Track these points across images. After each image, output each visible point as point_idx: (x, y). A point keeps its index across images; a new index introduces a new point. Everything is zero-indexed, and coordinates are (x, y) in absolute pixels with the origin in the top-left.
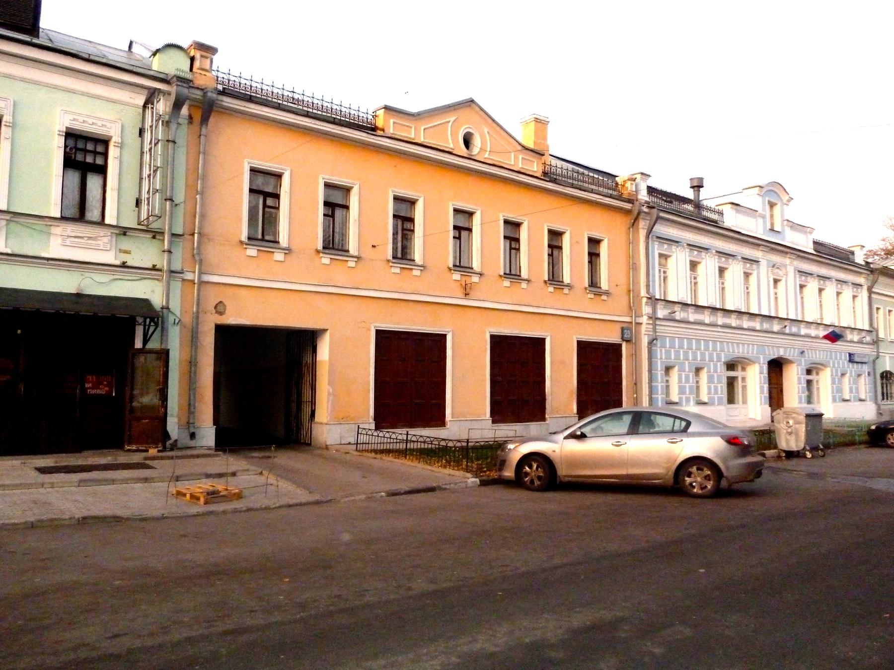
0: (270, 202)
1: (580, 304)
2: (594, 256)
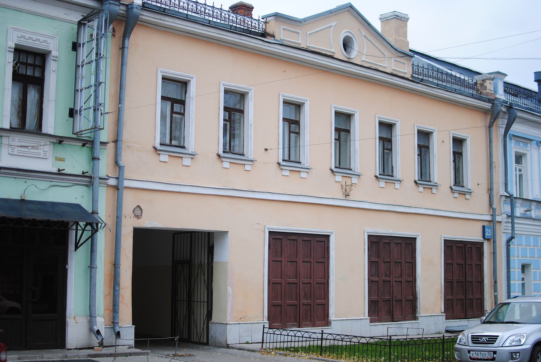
1: (443, 200)
2: (458, 155)
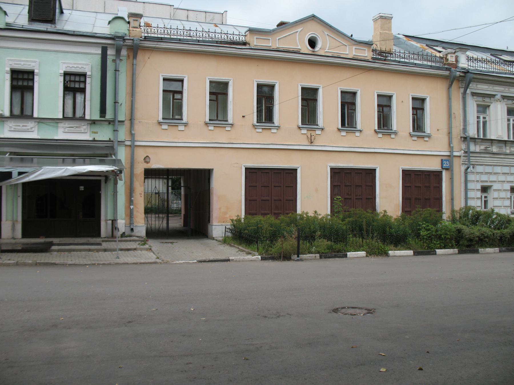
0: (177, 96)
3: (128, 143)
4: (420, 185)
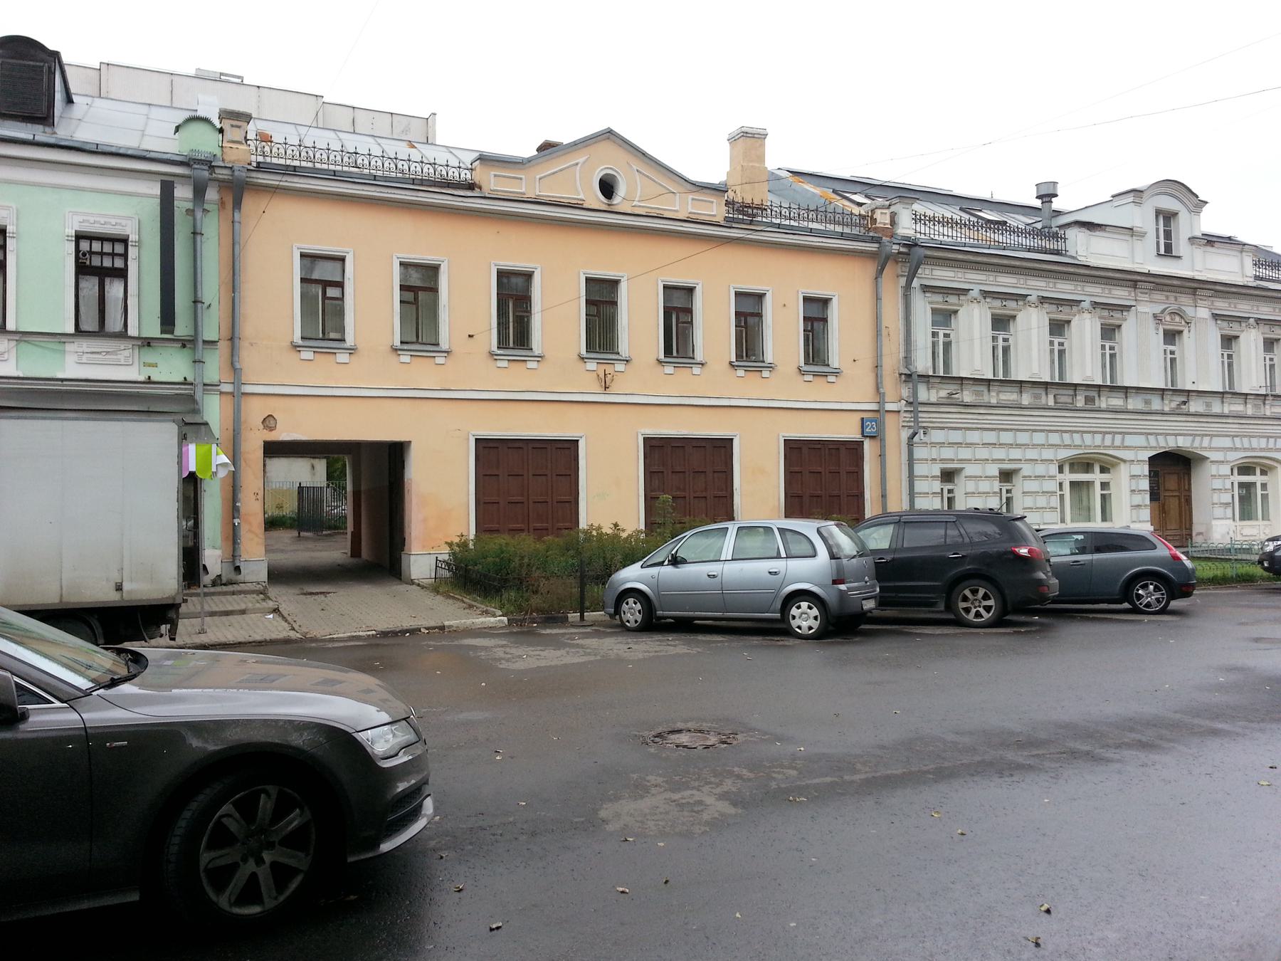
0: (331, 292)
3: (227, 388)
4: (819, 469)
